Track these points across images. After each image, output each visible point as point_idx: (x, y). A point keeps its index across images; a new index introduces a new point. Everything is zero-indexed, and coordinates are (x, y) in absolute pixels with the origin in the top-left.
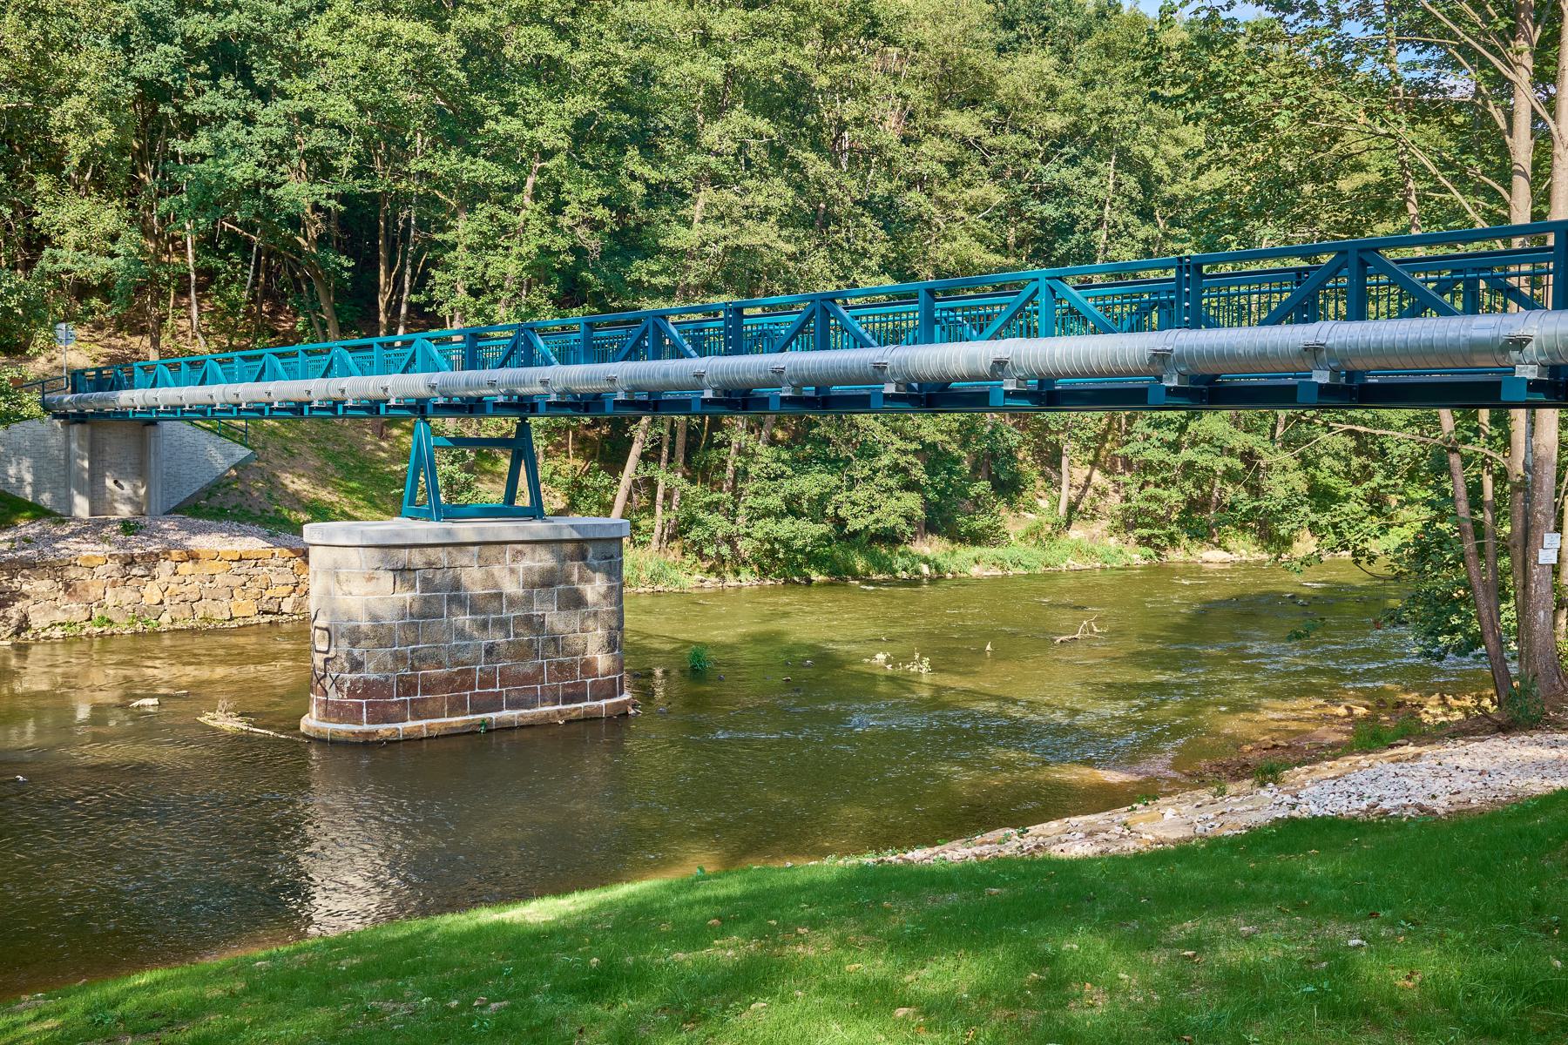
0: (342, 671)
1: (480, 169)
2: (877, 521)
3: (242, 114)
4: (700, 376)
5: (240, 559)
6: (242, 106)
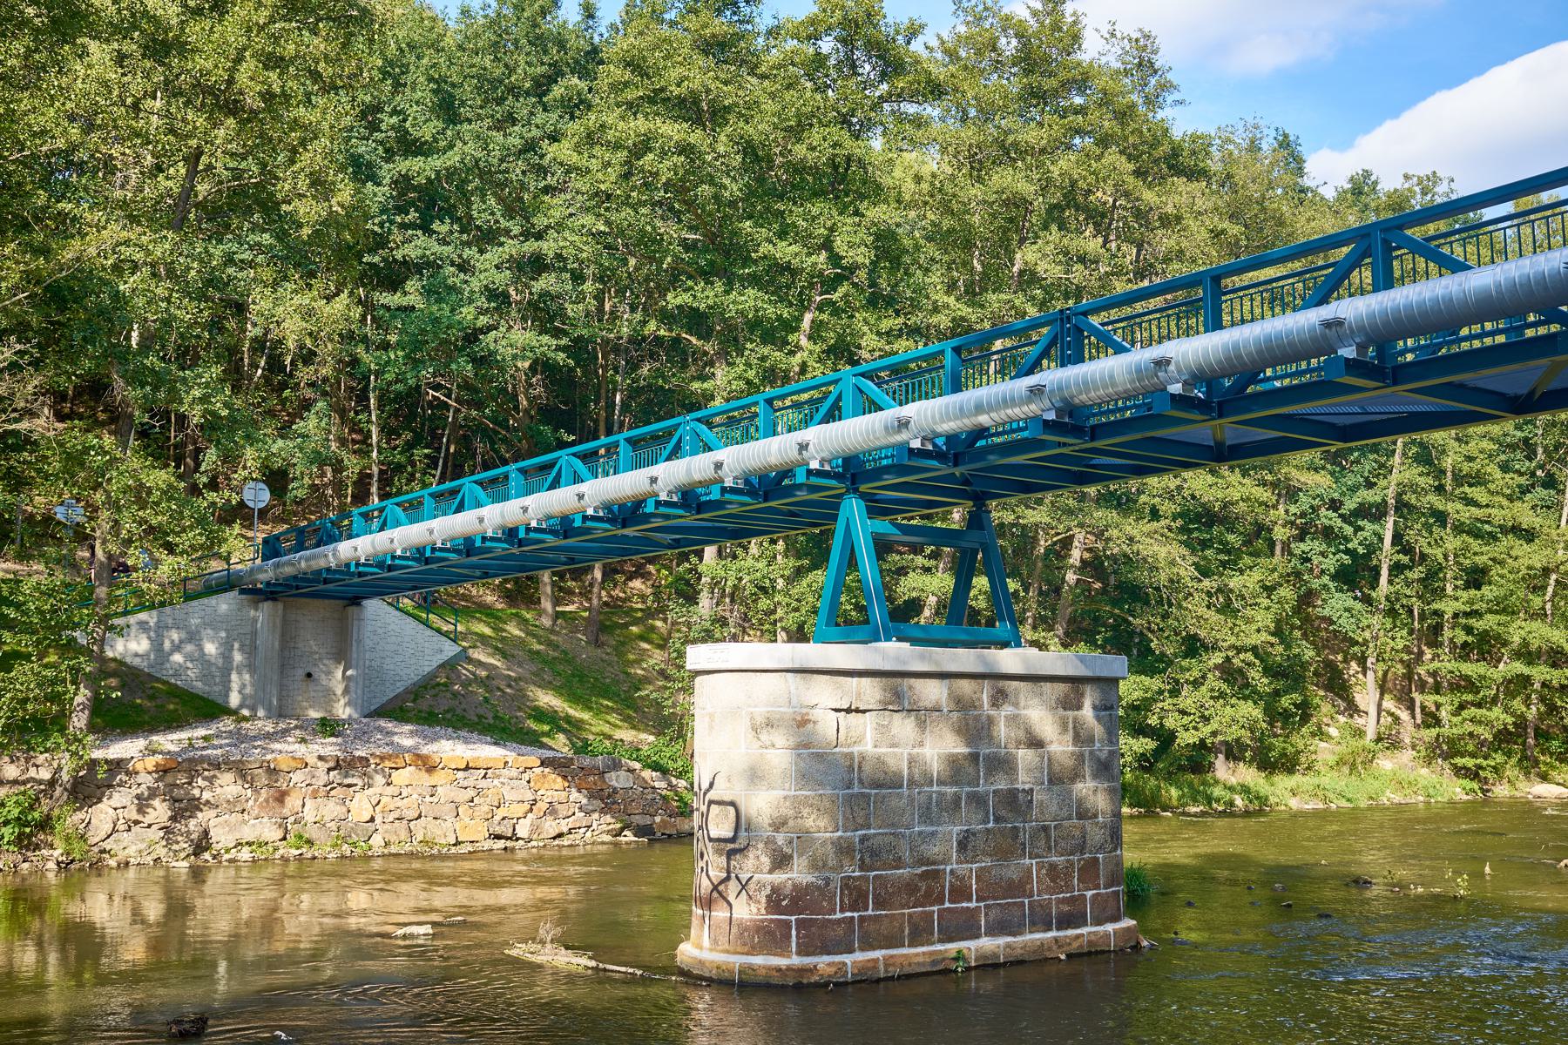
0: (758, 870)
1: (749, 300)
2: (1214, 734)
3: (457, 260)
5: (467, 768)
6: (459, 252)
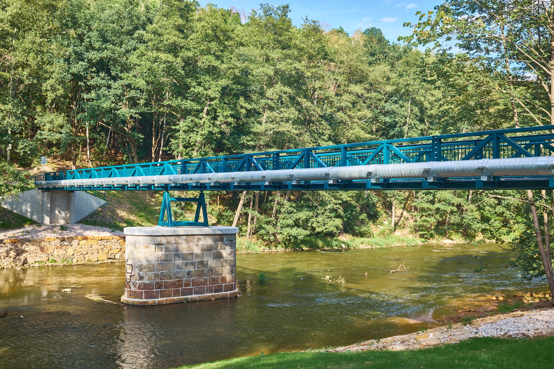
0: (136, 280)
2: (326, 229)
3: (107, 85)
5: (102, 240)
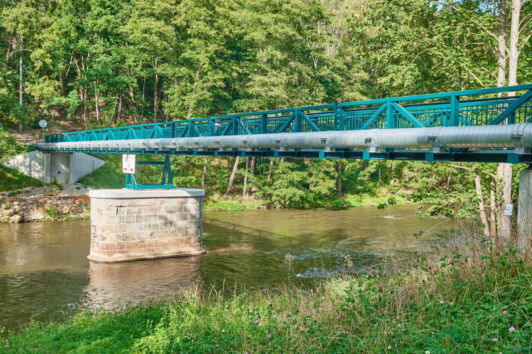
4: (278, 141)
